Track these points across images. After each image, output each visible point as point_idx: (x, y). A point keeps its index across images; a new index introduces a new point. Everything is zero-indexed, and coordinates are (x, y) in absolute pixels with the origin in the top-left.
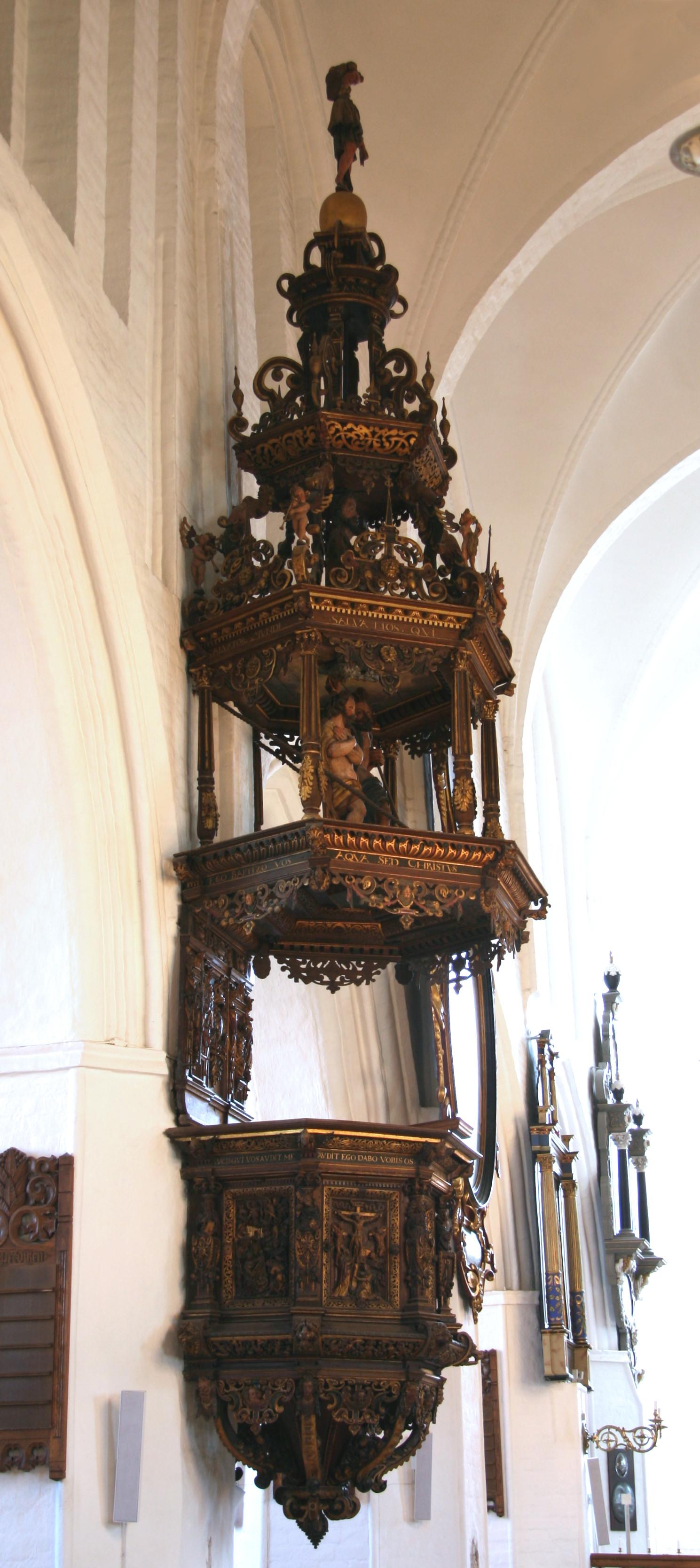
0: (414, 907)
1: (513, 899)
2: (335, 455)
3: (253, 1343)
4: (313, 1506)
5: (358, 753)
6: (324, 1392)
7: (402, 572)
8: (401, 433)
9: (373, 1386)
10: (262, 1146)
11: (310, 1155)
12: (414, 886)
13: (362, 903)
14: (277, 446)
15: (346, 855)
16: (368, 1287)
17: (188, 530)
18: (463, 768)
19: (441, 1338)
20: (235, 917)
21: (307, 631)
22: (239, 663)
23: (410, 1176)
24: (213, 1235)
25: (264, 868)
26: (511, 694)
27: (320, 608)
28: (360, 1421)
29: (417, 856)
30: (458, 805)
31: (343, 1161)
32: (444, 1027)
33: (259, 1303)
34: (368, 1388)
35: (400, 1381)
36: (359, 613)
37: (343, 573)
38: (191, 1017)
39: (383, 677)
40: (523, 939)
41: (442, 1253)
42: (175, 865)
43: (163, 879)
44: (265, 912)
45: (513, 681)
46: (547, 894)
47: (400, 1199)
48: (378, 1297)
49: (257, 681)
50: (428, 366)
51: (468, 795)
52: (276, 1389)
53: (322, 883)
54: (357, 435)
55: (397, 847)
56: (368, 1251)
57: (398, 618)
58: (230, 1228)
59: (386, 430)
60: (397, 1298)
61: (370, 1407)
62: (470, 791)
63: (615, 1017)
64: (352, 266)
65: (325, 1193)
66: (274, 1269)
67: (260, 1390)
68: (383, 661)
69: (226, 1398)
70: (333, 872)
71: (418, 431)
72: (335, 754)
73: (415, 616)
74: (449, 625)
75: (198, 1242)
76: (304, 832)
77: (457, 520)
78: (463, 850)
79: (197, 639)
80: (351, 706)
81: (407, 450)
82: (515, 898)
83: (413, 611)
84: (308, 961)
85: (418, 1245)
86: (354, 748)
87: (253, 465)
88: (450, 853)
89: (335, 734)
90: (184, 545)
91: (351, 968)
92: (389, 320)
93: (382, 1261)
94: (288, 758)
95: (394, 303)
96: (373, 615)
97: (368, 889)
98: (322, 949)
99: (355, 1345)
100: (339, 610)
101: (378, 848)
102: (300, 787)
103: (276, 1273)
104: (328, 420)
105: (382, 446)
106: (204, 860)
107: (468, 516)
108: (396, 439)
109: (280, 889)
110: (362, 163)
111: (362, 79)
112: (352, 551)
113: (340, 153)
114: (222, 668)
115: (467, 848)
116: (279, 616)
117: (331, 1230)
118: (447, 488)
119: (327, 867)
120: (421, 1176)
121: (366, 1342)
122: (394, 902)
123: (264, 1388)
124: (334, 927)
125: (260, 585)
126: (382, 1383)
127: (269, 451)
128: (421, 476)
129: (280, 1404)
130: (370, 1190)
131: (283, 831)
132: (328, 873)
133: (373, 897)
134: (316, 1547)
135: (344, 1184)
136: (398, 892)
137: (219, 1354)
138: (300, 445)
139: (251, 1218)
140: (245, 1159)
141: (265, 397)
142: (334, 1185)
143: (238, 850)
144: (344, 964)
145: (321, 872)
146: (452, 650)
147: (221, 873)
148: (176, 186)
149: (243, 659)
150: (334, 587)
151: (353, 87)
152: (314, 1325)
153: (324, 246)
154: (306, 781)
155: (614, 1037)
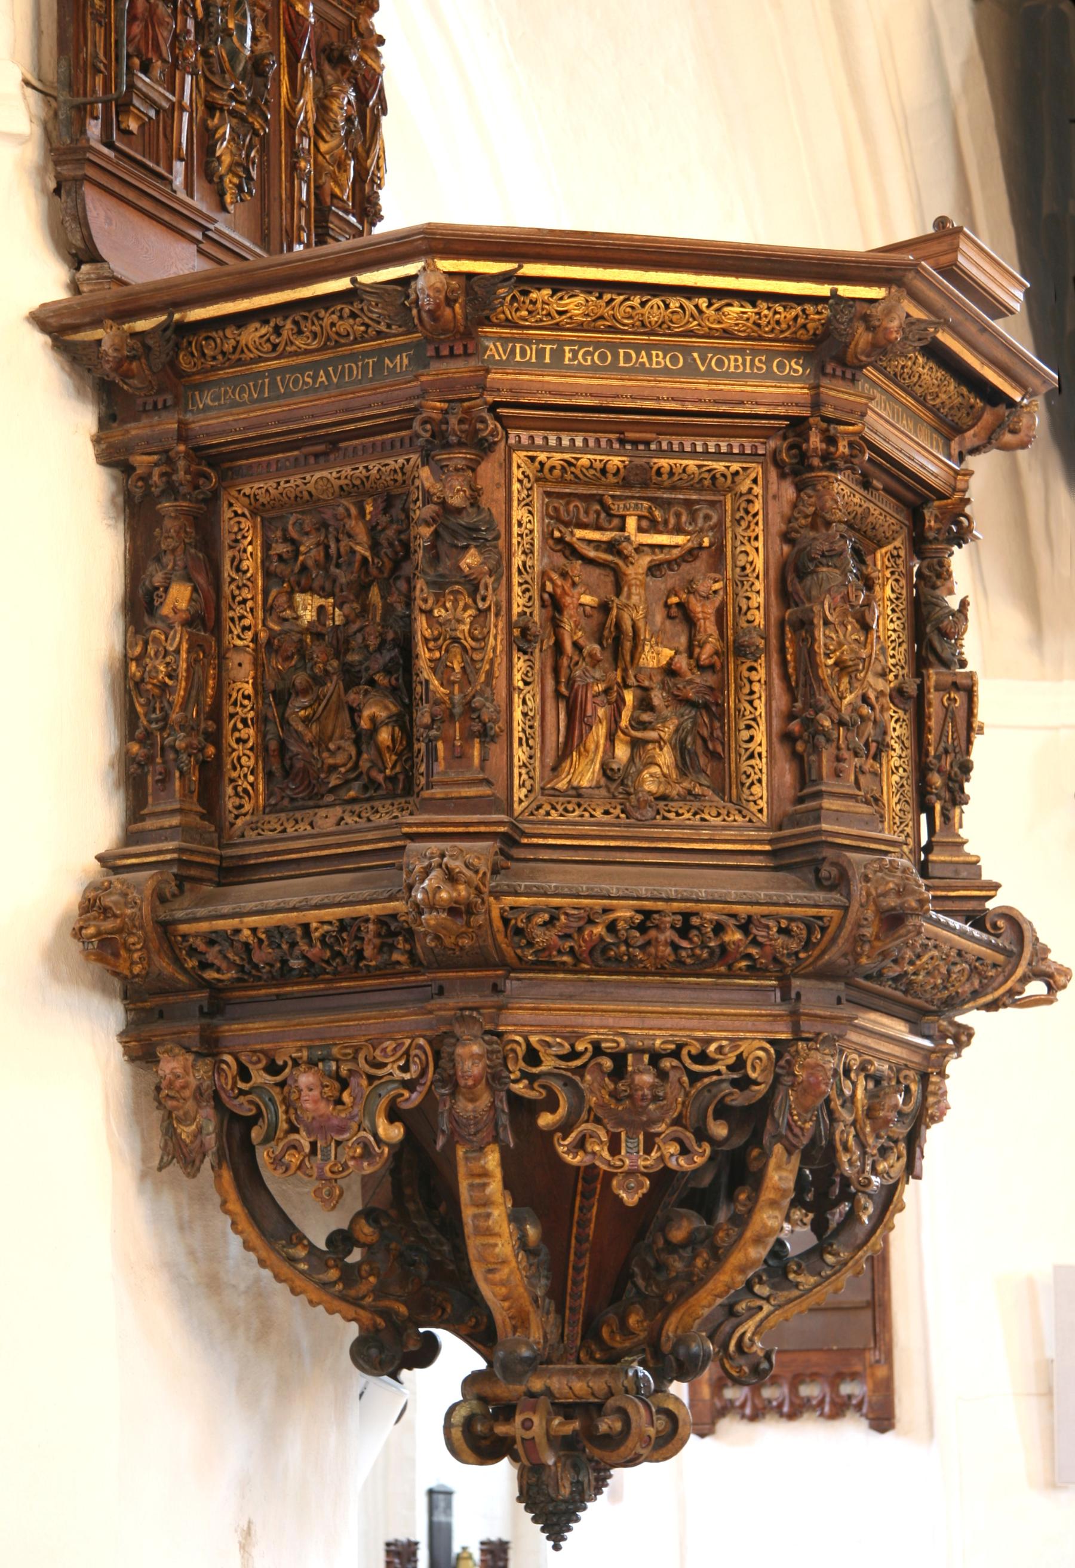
3: (299, 932)
4: (527, 1425)
6: (525, 1075)
9: (684, 1052)
10: (315, 335)
11: (459, 349)
16: (666, 757)
19: (892, 902)
23: (794, 412)
24: (188, 623)
28: (648, 1162)
31: (569, 367)
33: (327, 819)
34: (666, 1063)
35: (772, 1042)
41: (933, 675)
47: (766, 488)
48: (698, 790)
52: (380, 1072)
56: (668, 653)
58: (244, 601)
60: (760, 791)
61: (677, 1122)
65: (517, 473)
66: (366, 713)
67: (337, 1077)
69: (243, 1107)
75: (146, 643)
85: (818, 621)
93: (710, 679)
99: (612, 927)
103: (376, 725)
117: (543, 588)
120: (829, 412)
121: (647, 920)
123: (344, 1070)
126: (713, 1047)
129: (394, 1115)
130: (664, 463)
134: (556, 1548)
135: (579, 442)
137: (210, 975)
139: (304, 568)
140: (273, 385)
142: (546, 448)
152: (467, 865)
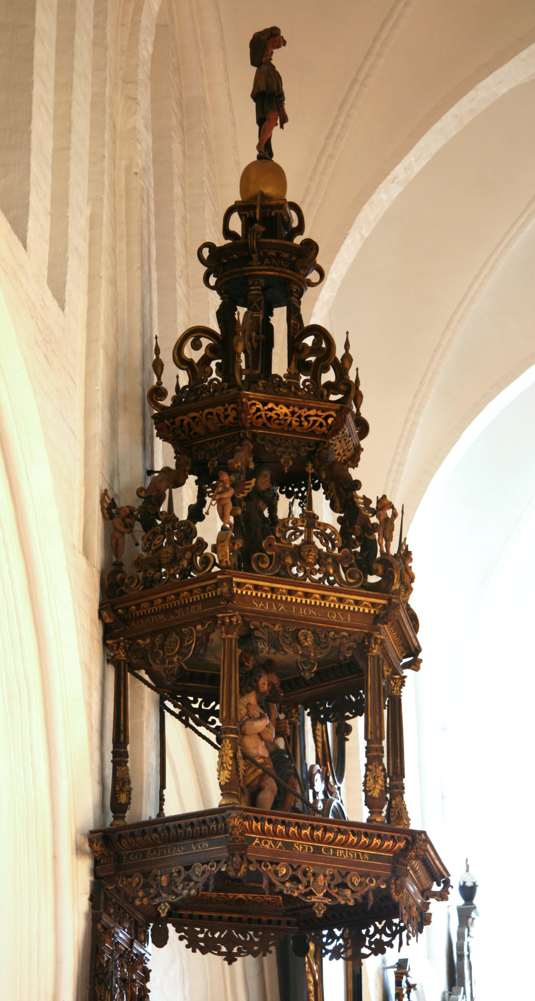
0: (327, 895)
1: (418, 883)
2: (254, 433)
5: (270, 731)
7: (321, 558)
8: (320, 413)
12: (327, 873)
13: (277, 890)
14: (197, 420)
15: (263, 842)
17: (108, 501)
18: (375, 754)
20: (150, 897)
21: (229, 614)
22: (158, 639)
25: (180, 849)
26: (417, 669)
27: (242, 592)
29: (330, 843)
30: (370, 791)
32: (317, 977)
36: (279, 598)
37: (265, 559)
38: (101, 996)
39: (300, 662)
40: (425, 921)
42: (91, 842)
43: (77, 854)
44: (181, 894)
45: (420, 656)
46: (449, 875)
49: (175, 659)
50: (347, 345)
51: (380, 782)
53: (240, 870)
54: (277, 414)
55: (312, 835)
57: (316, 602)
59: (306, 410)
62: (382, 777)
63: (470, 934)
64: (273, 241)
68: (301, 645)
70: (250, 859)
71: (336, 411)
72: (248, 732)
73: (332, 601)
74: (364, 610)
76: (224, 819)
77: (373, 505)
78: (375, 839)
79: (115, 611)
80: (264, 683)
81: (324, 429)
82: (419, 880)
83: (330, 596)
84: (206, 930)
86: (267, 726)
87: (171, 435)
88: (362, 841)
89: (248, 711)
90: (104, 516)
91: (248, 939)
92: (306, 289)
94: (191, 722)
95: (312, 271)
96: (292, 599)
97: (283, 876)
98: (220, 918)
100: (259, 595)
101: (294, 837)
102: (219, 771)
104: (250, 399)
105: (301, 425)
106: (120, 837)
107: (385, 502)
108: (315, 418)
109: (197, 873)
110: (282, 127)
111: (284, 43)
112: (273, 537)
113: (261, 121)
114: (140, 641)
115: (379, 837)
116: (200, 597)
118: (359, 459)
119: (244, 854)
122: (308, 890)
124: (237, 897)
125: (183, 566)
127: (189, 424)
128: (336, 450)
131: (201, 816)
132: (245, 859)
133: (288, 885)
136: (312, 880)
138: (220, 421)
141: (185, 367)
143: (155, 830)
144: (241, 935)
145: (239, 859)
146: (366, 634)
147: (135, 851)
148: (104, 156)
149: (161, 635)
150: (256, 572)
151: (275, 51)
153: (245, 215)
154: (225, 765)
155: (468, 956)
